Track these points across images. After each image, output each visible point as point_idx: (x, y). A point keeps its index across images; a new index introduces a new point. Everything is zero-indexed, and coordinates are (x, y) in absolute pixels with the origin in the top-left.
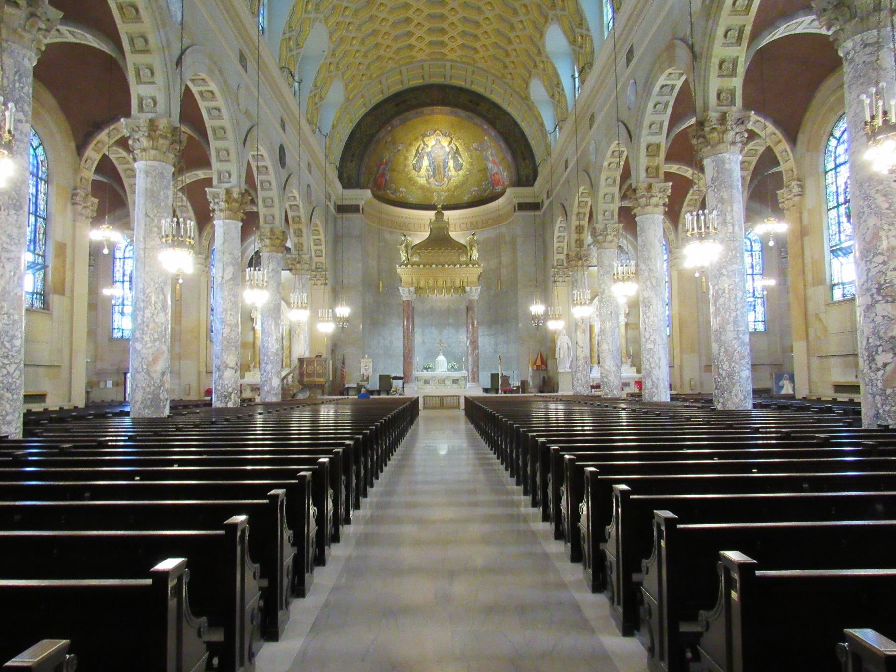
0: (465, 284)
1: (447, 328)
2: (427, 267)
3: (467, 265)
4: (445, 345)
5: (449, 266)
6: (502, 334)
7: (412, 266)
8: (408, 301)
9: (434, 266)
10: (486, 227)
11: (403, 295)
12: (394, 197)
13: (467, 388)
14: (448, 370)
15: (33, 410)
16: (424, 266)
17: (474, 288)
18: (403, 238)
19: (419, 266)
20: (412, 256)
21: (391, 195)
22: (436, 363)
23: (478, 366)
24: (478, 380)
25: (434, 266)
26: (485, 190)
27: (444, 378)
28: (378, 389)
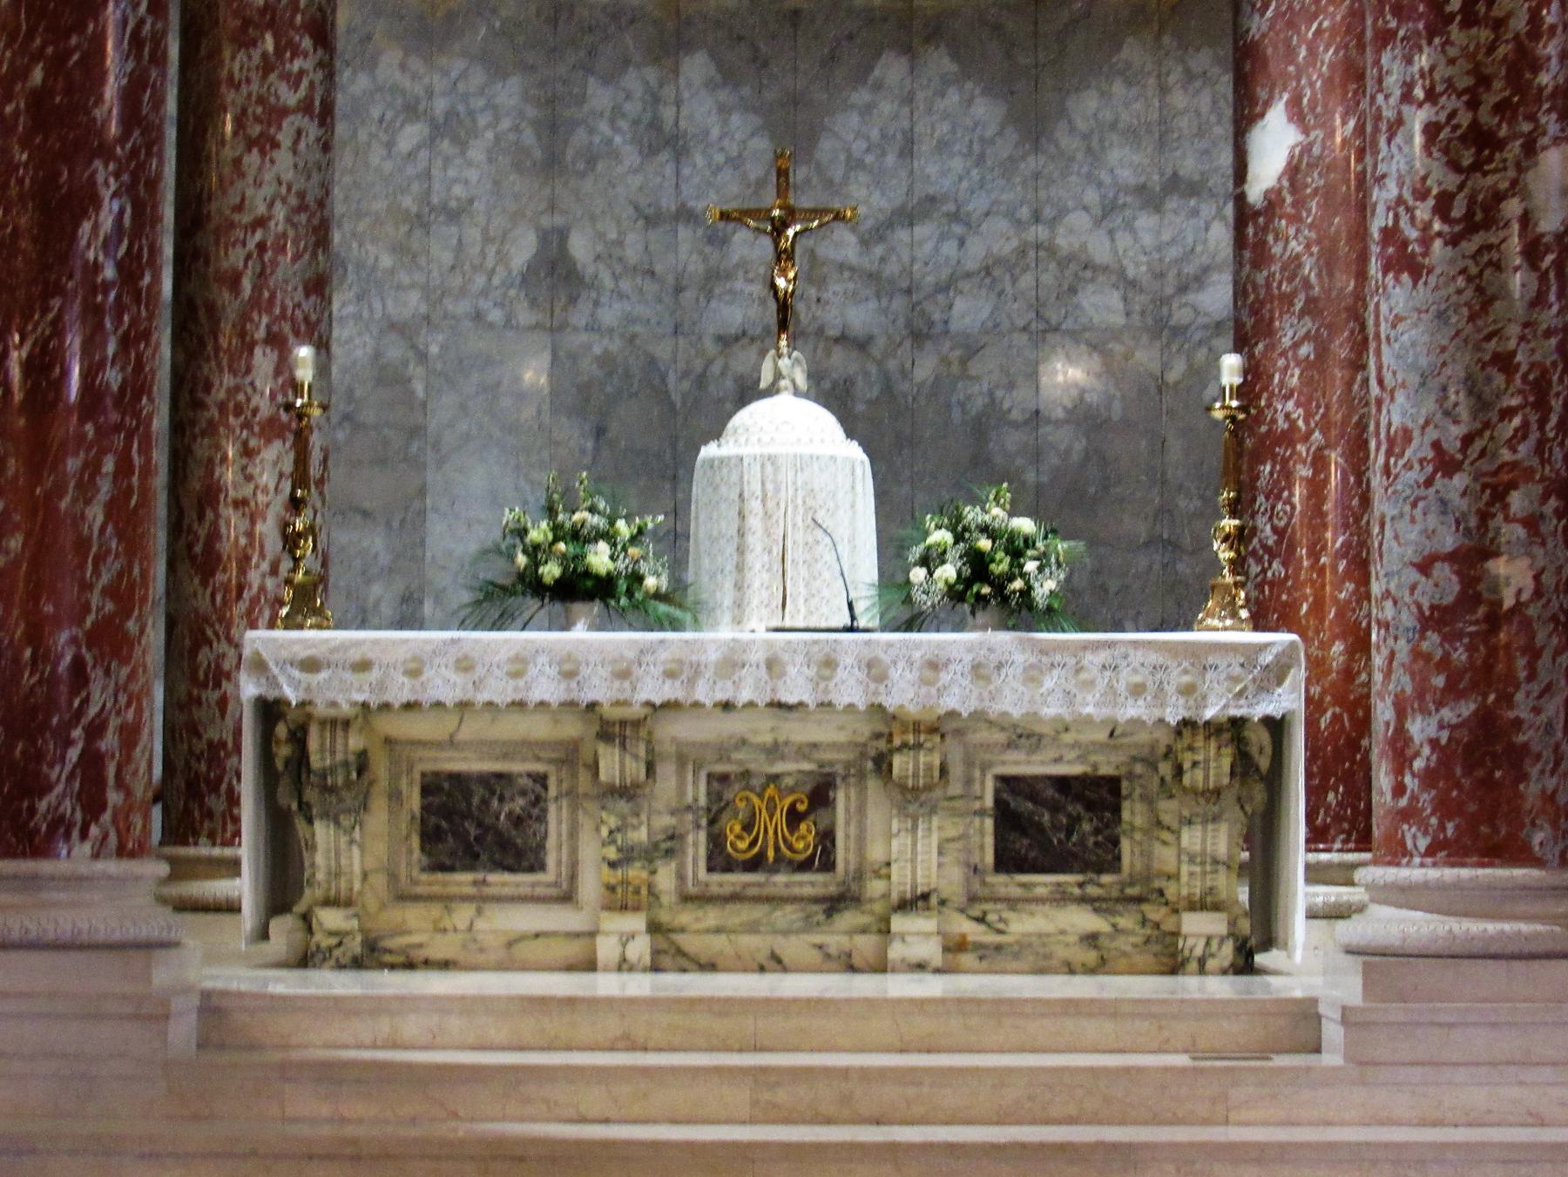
1: (892, 69)
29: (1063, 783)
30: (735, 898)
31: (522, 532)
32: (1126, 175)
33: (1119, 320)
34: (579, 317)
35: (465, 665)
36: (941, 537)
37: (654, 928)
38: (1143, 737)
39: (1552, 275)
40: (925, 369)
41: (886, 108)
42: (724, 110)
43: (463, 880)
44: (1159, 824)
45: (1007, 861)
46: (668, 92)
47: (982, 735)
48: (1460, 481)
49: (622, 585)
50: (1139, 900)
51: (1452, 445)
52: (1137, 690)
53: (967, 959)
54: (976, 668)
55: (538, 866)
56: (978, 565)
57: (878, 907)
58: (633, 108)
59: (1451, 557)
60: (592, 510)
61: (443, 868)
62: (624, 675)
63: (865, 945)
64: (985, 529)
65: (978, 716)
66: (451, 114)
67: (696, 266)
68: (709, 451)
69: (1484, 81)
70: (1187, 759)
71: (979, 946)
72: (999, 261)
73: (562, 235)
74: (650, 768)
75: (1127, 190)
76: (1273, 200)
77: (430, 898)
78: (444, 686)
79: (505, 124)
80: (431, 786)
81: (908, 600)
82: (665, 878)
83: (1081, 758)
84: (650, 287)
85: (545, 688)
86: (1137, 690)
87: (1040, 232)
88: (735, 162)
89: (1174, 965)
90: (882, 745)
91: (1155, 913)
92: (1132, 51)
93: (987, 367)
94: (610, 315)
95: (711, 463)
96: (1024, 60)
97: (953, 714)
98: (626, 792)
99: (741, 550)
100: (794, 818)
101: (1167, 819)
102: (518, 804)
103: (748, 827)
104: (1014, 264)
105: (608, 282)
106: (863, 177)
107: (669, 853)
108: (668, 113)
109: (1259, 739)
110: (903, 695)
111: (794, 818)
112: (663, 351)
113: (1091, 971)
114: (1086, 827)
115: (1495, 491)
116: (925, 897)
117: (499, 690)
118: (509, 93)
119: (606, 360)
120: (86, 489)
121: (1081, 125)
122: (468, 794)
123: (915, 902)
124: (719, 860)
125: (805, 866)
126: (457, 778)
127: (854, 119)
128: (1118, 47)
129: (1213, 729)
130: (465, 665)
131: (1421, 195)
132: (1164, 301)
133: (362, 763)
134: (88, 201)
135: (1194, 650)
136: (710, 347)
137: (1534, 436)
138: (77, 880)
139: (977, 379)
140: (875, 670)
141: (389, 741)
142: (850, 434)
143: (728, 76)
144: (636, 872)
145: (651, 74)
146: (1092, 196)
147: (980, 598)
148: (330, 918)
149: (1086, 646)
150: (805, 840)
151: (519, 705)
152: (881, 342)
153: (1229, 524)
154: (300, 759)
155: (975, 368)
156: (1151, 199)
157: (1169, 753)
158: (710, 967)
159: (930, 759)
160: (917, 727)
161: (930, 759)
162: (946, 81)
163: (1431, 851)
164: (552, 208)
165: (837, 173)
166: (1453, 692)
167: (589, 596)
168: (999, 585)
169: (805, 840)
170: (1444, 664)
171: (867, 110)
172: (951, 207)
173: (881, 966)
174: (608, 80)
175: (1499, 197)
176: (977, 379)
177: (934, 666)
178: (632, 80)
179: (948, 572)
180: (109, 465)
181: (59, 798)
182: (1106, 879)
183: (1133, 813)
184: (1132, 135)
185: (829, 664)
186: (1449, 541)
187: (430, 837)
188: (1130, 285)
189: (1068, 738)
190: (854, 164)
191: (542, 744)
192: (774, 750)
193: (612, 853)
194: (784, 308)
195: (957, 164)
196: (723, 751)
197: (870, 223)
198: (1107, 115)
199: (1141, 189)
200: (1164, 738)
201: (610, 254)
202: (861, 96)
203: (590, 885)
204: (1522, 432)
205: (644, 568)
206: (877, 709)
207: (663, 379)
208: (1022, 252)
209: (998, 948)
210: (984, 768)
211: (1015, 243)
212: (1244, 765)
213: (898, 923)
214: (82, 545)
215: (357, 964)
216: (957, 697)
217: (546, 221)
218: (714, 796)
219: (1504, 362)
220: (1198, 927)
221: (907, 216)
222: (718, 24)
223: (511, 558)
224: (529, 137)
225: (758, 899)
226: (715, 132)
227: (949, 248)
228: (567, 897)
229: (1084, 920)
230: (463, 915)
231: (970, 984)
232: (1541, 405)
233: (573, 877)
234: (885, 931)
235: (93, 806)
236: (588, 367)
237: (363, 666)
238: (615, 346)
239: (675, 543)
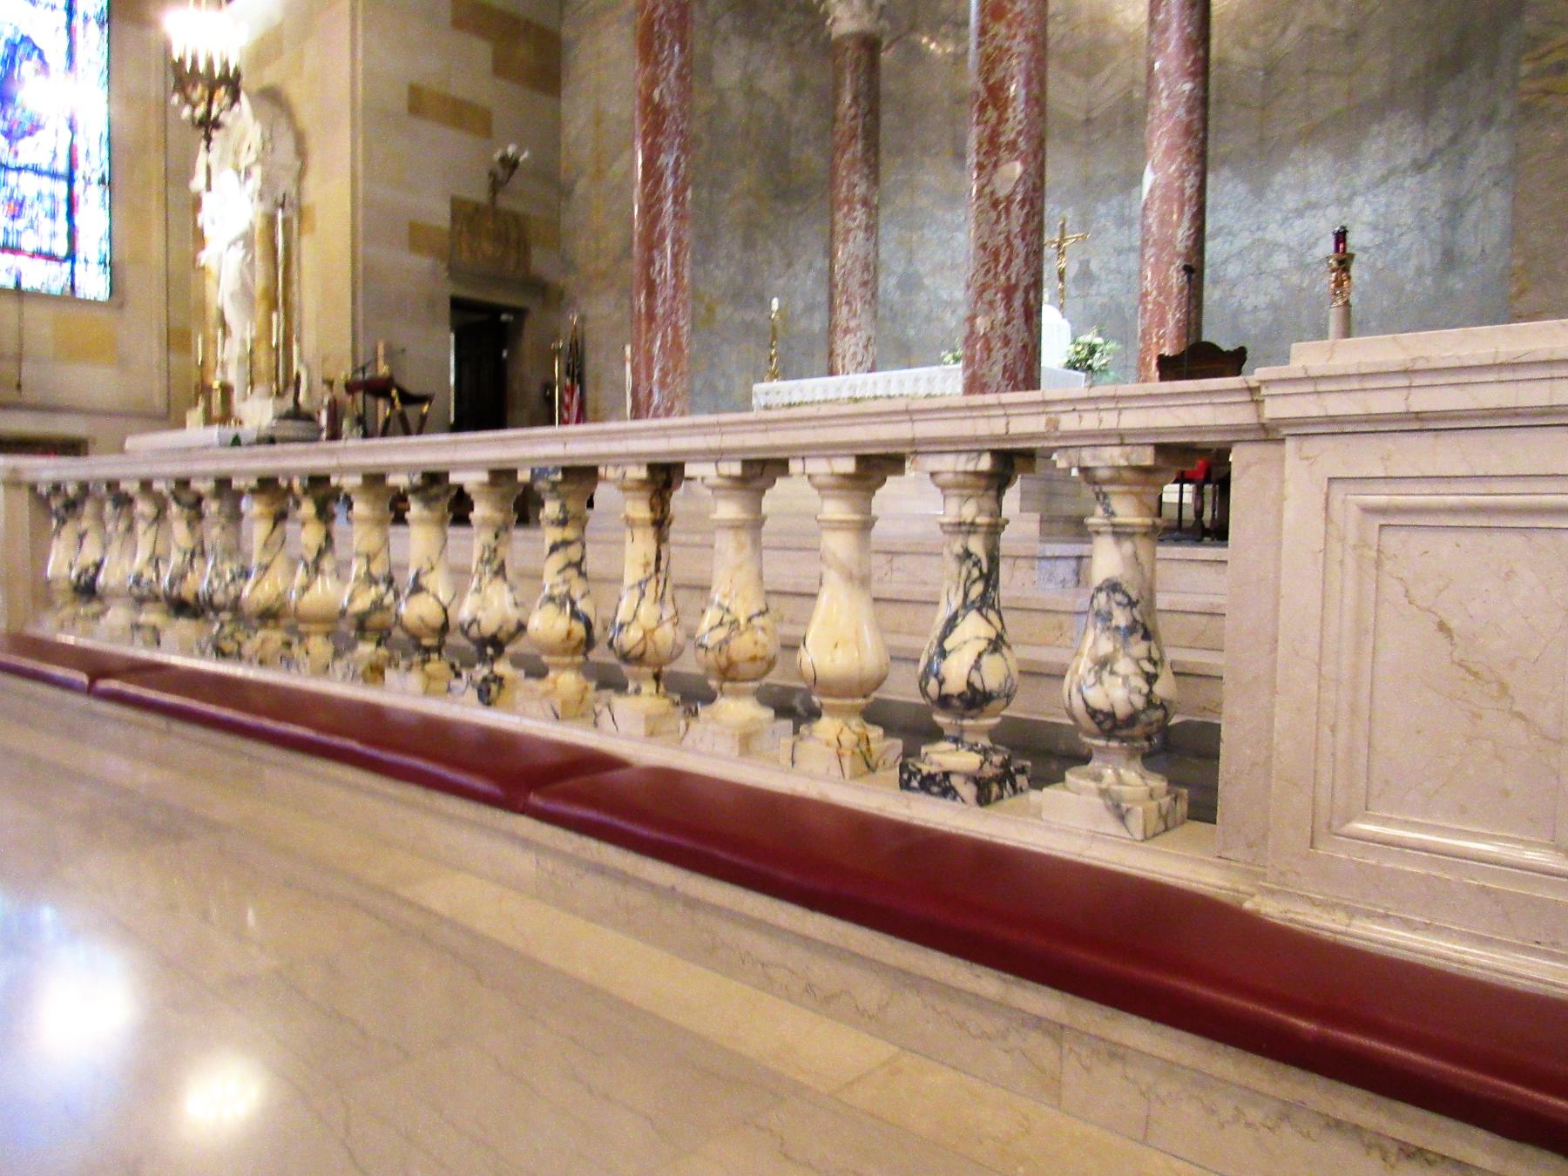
32: (1291, 205)
33: (1286, 265)
34: (1093, 291)
39: (1003, 213)
46: (1127, 203)
54: (929, 379)
72: (1245, 248)
73: (1088, 261)
84: (1119, 276)
87: (1259, 234)
92: (1296, 154)
93: (1239, 291)
94: (1104, 289)
104: (1249, 249)
108: (1127, 211)
112: (1123, 300)
119: (1103, 306)
132: (1303, 255)
139: (1234, 296)
146: (1279, 217)
155: (1235, 291)
156: (1299, 213)
172: (1227, 230)
176: (1234, 296)
178: (1114, 202)
188: (1290, 250)
195: (1231, 212)
208: (1253, 243)
211: (1249, 241)
217: (1081, 258)
227: (1227, 246)
237: (778, 393)
238: (1106, 300)
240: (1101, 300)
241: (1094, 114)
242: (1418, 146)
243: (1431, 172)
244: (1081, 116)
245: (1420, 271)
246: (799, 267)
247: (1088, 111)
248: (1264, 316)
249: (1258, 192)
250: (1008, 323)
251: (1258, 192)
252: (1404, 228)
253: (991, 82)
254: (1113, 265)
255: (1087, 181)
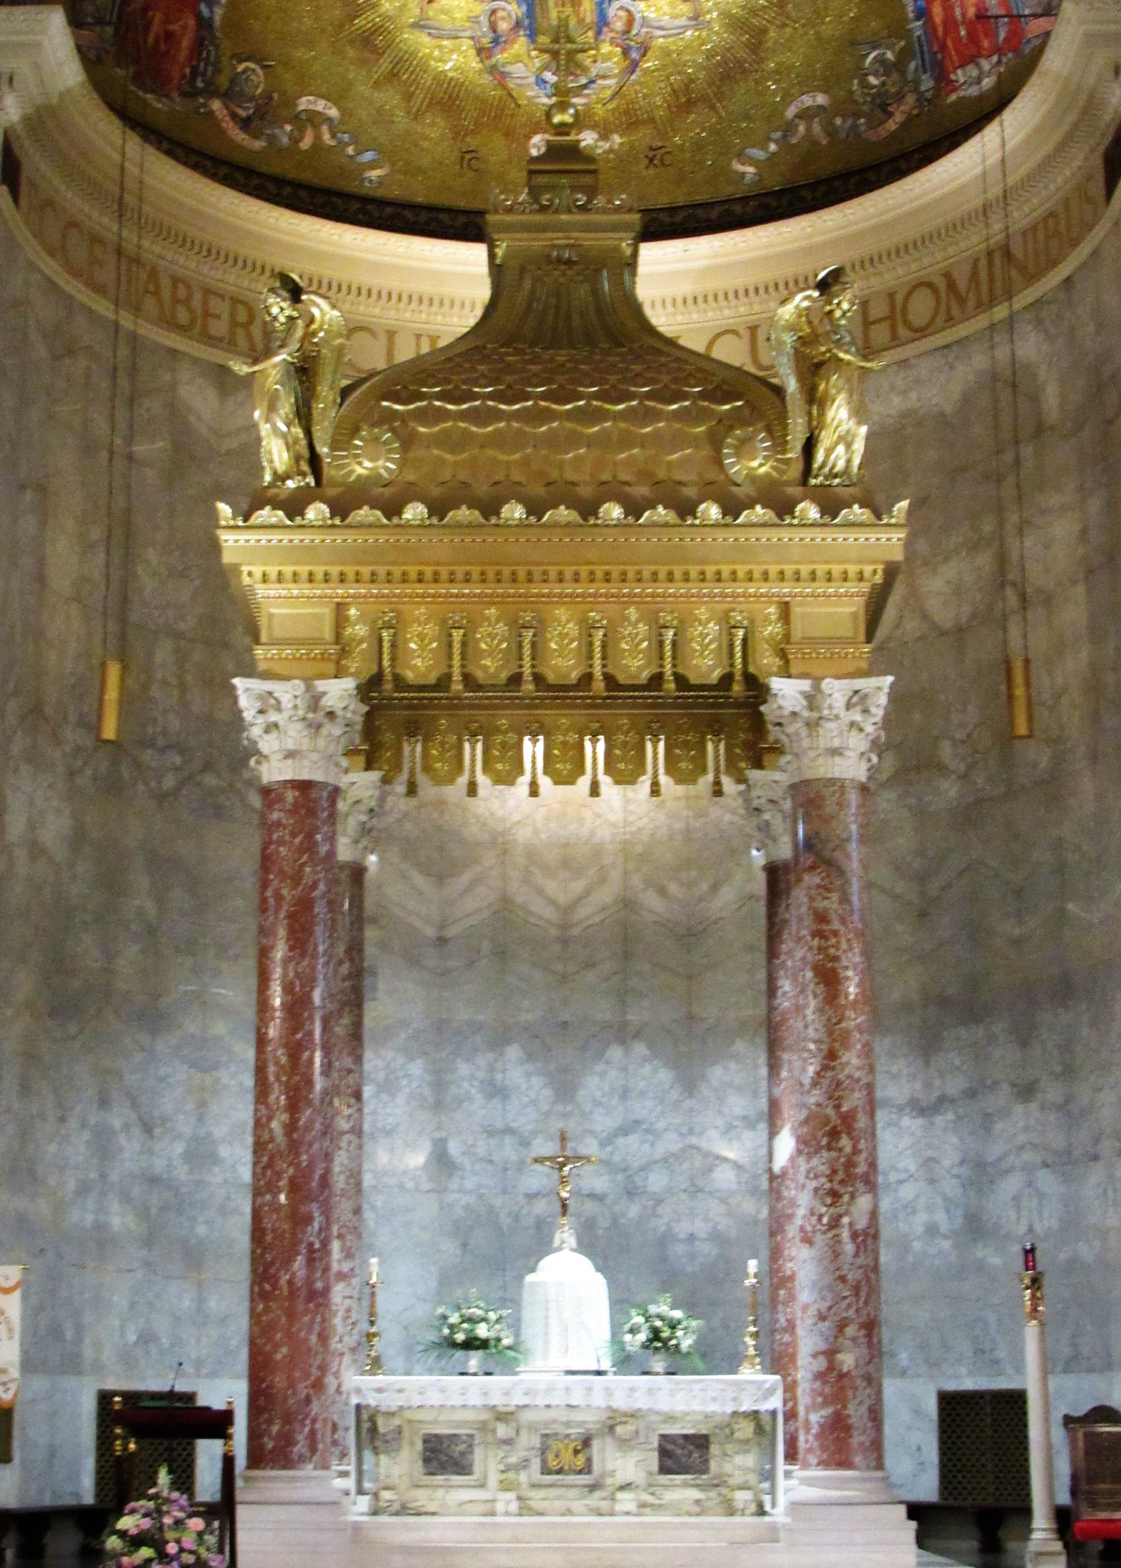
0: (767, 660)
1: (615, 1052)
2: (464, 514)
3: (784, 508)
4: (599, 1183)
5: (634, 509)
6: (1026, 1091)
7: (341, 509)
8: (304, 786)
9: (514, 511)
10: (895, 341)
11: (268, 744)
12: (259, 145)
13: (779, 1514)
14: (625, 1363)
15: (202, 1401)
16: (438, 509)
17: (836, 690)
18: (279, 308)
19: (392, 509)
20: (343, 439)
21: (238, 136)
22: (530, 1313)
23: (870, 1327)
24: (877, 1446)
25: (514, 511)
26: (882, 104)
27: (591, 1419)
28: (88, 1497)
29: (686, 1437)
30: (551, 1486)
31: (445, 1317)
32: (738, 1111)
34: (454, 1185)
35: (443, 1391)
36: (640, 1319)
37: (520, 1498)
38: (719, 1419)
40: (634, 1211)
41: (613, 1073)
42: (528, 1075)
43: (439, 1479)
44: (726, 1455)
45: (664, 1470)
47: (653, 1418)
48: (827, 1324)
49: (492, 1343)
50: (717, 1486)
51: (823, 1310)
52: (714, 1399)
53: (647, 1510)
55: (469, 1473)
56: (656, 1333)
57: (611, 1489)
58: (481, 1074)
59: (823, 1353)
60: (477, 1307)
61: (433, 1474)
62: (507, 1394)
63: (605, 1505)
64: (661, 1318)
65: (650, 1410)
66: (387, 1080)
67: (514, 1157)
68: (530, 1278)
69: (834, 1172)
70: (736, 1427)
71: (652, 1505)
72: (673, 1155)
74: (518, 1431)
75: (737, 1118)
76: (784, 1173)
77: (426, 1486)
78: (434, 1399)
79: (415, 1084)
80: (428, 1440)
81: (623, 1350)
82: (523, 1477)
83: (693, 1427)
84: (489, 1167)
85: (475, 1400)
86: (714, 1399)
88: (534, 1102)
89: (731, 1511)
90: (610, 1422)
91: (724, 1491)
93: (666, 1210)
94: (470, 1183)
95: (532, 1284)
96: (684, 1049)
97: (639, 1410)
98: (508, 1442)
99: (547, 1326)
100: (576, 1452)
101: (729, 1452)
102: (462, 1447)
103: (557, 1456)
105: (468, 1167)
106: (601, 1110)
107: (525, 1467)
108: (499, 1077)
109: (766, 1419)
110: (621, 1402)
111: (576, 1452)
112: (497, 1202)
113: (698, 1515)
114: (696, 1455)
115: (841, 1326)
116: (629, 1485)
117: (457, 1401)
118: (417, 1068)
119: (467, 1208)
120: (310, 1330)
121: (715, 1084)
122: (442, 1443)
123: (624, 1487)
124: (546, 1470)
125: (580, 1472)
126: (436, 1436)
127: (597, 1079)
128: (733, 1042)
129: (746, 1415)
130: (443, 1391)
131: (812, 1214)
133: (399, 1431)
134: (309, 1219)
135: (737, 1383)
136: (522, 1200)
137: (854, 1308)
138: (308, 1478)
139: (660, 1216)
140: (608, 1391)
141: (410, 1421)
142: (598, 1269)
143: (530, 1057)
144: (511, 1475)
145: (490, 1056)
146: (720, 1122)
147: (656, 1349)
148: (386, 1495)
149: (694, 1382)
150: (580, 1461)
151: (464, 1406)
152: (611, 1197)
153: (752, 1329)
154: (373, 1430)
157: (729, 1425)
158: (541, 1514)
159: (630, 1428)
160: (625, 1414)
161: (630, 1428)
162: (645, 1060)
163: (818, 1464)
164: (439, 1128)
165: (587, 1107)
166: (825, 1404)
167: (477, 1348)
168: (665, 1342)
169: (580, 1461)
170: (821, 1394)
171: (602, 1074)
173: (612, 1514)
174: (469, 1059)
175: (841, 1216)
176: (660, 1216)
177: (632, 1390)
179: (642, 1337)
180: (318, 1320)
181: (300, 1447)
182: (704, 1477)
183: (714, 1449)
184: (740, 1089)
185: (590, 1389)
186: (822, 1346)
187: (427, 1461)
189: (689, 1418)
190: (597, 1103)
191: (473, 1422)
192: (568, 1424)
193: (502, 1467)
194: (564, 1207)
195: (649, 1104)
196: (546, 1424)
197: (605, 1134)
198: (727, 1079)
199: (745, 1118)
200: (727, 1419)
201: (467, 1153)
202: (599, 1067)
203: (493, 1479)
204: (849, 1306)
205: (502, 1334)
206: (609, 1408)
207: (497, 1215)
209: (660, 1506)
210: (654, 1430)
211: (680, 1145)
212: (759, 1430)
213: (620, 1495)
214: (309, 1350)
215: (397, 1514)
216: (641, 1402)
218: (543, 1443)
219: (843, 1279)
220: (742, 1497)
221: (624, 1130)
222: (526, 1029)
223: (440, 1330)
224: (427, 1091)
225: (563, 1486)
226: (523, 1087)
227: (647, 1146)
228: (482, 1486)
229: (694, 1494)
230: (440, 1493)
231: (650, 1518)
232: (857, 1294)
233: (485, 1477)
234: (613, 1499)
235: (313, 1449)
236: (459, 1212)
237: (400, 1391)
238: (472, 1199)
239: (516, 1326)
240: (465, 1200)
241: (451, 932)
242: (918, 1085)
243: (938, 1120)
244: (430, 932)
245: (932, 1230)
246: (73, 1123)
247: (442, 927)
248: (707, 1249)
249: (689, 1084)
250: (869, 1362)
251: (689, 1084)
252: (903, 1176)
253: (844, 1109)
254: (481, 1151)
255: (440, 1026)
